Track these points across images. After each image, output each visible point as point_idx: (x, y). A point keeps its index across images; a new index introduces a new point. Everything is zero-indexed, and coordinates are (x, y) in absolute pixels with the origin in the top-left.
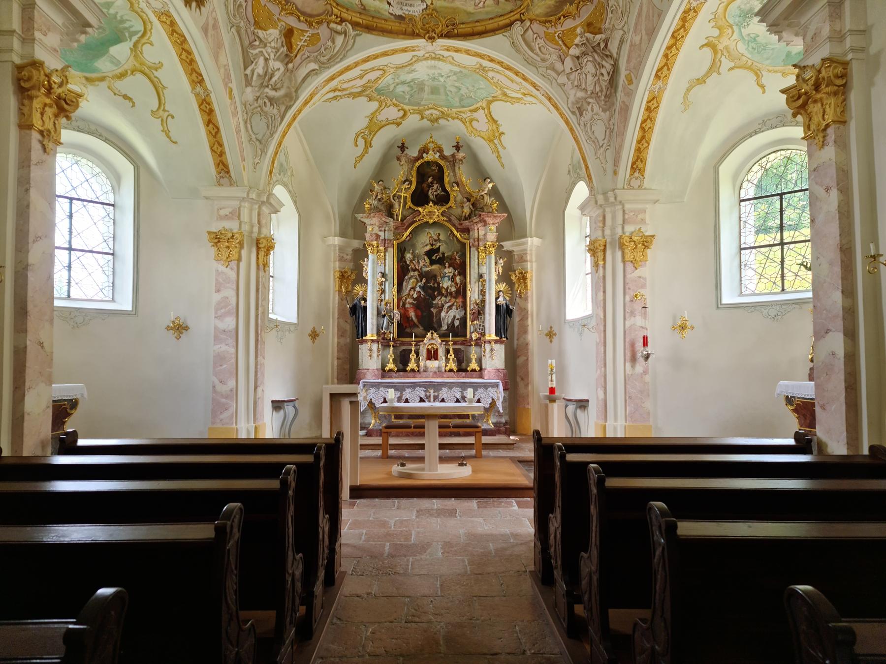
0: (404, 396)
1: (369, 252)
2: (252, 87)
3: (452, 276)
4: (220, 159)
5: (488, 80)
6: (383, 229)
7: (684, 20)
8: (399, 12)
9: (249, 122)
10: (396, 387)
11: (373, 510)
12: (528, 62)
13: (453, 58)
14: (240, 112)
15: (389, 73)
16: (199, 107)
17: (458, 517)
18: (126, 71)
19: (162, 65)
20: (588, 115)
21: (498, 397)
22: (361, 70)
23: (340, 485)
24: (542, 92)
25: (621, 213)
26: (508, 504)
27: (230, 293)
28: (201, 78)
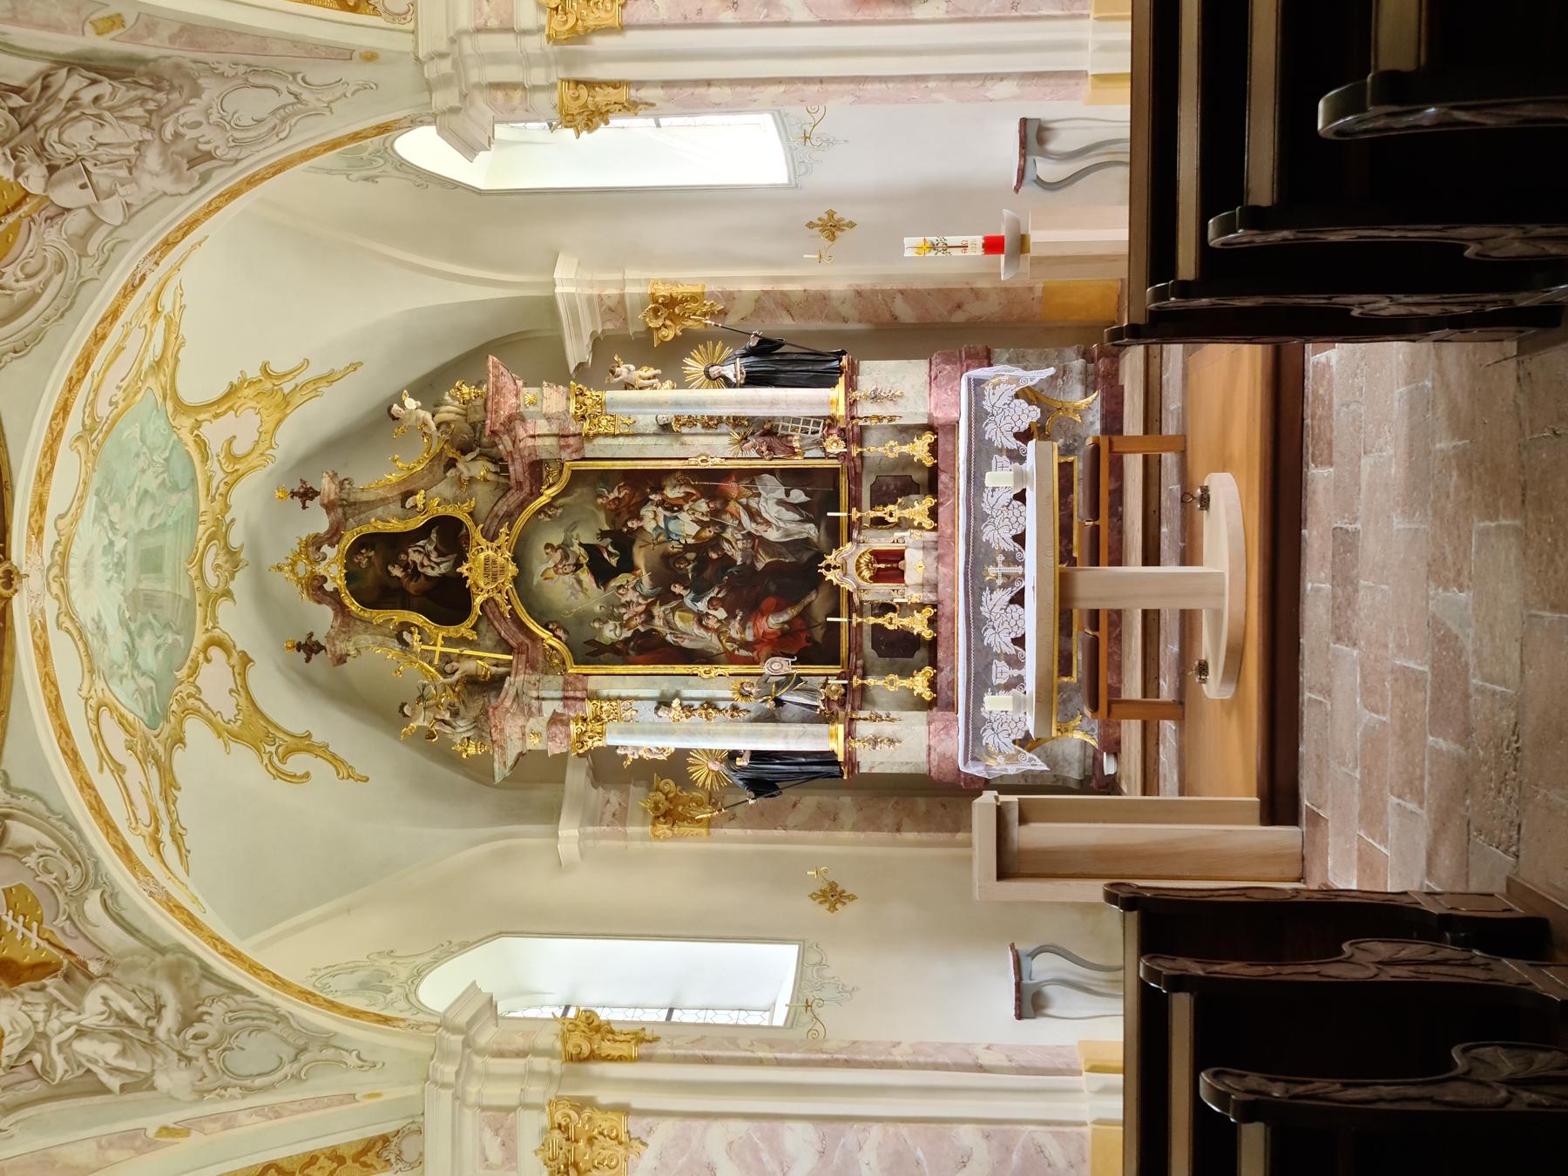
0: (1006, 649)
1: (600, 744)
2: (153, 1071)
3: (666, 509)
4: (349, 1162)
5: (119, 415)
6: (535, 703)
9: (248, 1082)
10: (980, 683)
11: (1333, 764)
12: (67, 310)
13: (62, 516)
14: (224, 1107)
15: (107, 692)
17: (1358, 525)
20: (211, 138)
21: (1009, 382)
22: (101, 769)
23: (1279, 53)
24: (150, 264)
25: (483, 39)
26: (1323, 377)
27: (718, 1134)
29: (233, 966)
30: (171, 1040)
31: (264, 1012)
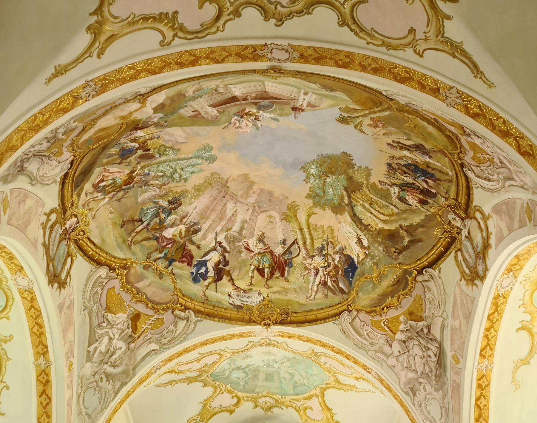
2: (92, 362)
5: (321, 366)
7: (495, 304)
8: (238, 303)
9: (82, 395)
13: (287, 344)
19: (13, 337)
20: (421, 395)
22: (199, 354)
24: (374, 375)
28: (45, 350)
30: (102, 369)
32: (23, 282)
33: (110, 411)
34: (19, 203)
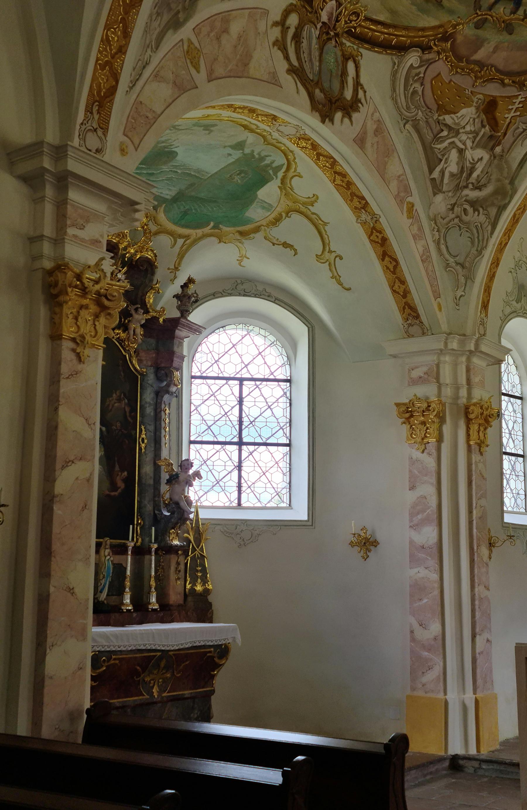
2: (444, 192)
4: (404, 300)
9: (442, 241)
14: (427, 231)
16: (369, 238)
18: (281, 215)
19: (318, 198)
27: (429, 490)
28: (364, 202)
29: (508, 221)
30: (462, 198)
31: (483, 242)
32: (290, 130)
33: (492, 251)
34: (218, 38)
